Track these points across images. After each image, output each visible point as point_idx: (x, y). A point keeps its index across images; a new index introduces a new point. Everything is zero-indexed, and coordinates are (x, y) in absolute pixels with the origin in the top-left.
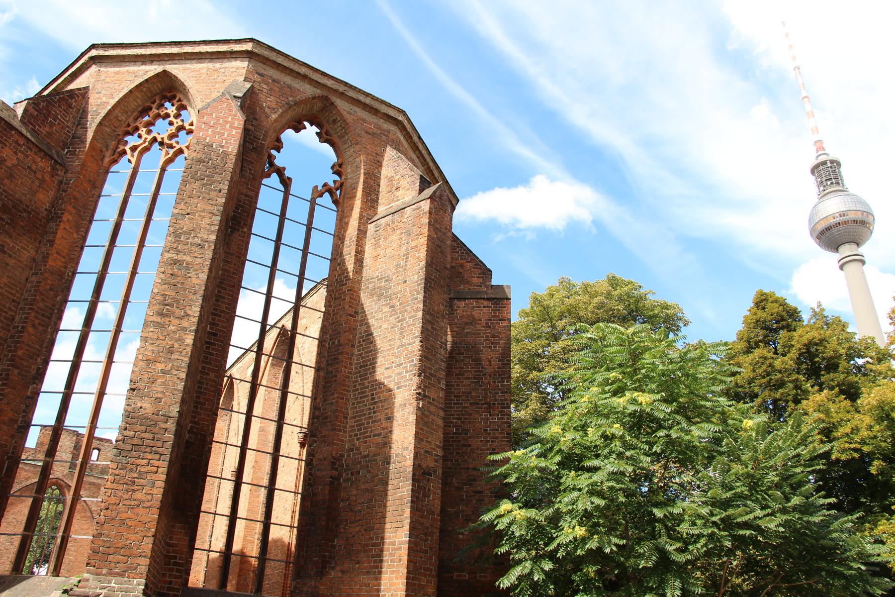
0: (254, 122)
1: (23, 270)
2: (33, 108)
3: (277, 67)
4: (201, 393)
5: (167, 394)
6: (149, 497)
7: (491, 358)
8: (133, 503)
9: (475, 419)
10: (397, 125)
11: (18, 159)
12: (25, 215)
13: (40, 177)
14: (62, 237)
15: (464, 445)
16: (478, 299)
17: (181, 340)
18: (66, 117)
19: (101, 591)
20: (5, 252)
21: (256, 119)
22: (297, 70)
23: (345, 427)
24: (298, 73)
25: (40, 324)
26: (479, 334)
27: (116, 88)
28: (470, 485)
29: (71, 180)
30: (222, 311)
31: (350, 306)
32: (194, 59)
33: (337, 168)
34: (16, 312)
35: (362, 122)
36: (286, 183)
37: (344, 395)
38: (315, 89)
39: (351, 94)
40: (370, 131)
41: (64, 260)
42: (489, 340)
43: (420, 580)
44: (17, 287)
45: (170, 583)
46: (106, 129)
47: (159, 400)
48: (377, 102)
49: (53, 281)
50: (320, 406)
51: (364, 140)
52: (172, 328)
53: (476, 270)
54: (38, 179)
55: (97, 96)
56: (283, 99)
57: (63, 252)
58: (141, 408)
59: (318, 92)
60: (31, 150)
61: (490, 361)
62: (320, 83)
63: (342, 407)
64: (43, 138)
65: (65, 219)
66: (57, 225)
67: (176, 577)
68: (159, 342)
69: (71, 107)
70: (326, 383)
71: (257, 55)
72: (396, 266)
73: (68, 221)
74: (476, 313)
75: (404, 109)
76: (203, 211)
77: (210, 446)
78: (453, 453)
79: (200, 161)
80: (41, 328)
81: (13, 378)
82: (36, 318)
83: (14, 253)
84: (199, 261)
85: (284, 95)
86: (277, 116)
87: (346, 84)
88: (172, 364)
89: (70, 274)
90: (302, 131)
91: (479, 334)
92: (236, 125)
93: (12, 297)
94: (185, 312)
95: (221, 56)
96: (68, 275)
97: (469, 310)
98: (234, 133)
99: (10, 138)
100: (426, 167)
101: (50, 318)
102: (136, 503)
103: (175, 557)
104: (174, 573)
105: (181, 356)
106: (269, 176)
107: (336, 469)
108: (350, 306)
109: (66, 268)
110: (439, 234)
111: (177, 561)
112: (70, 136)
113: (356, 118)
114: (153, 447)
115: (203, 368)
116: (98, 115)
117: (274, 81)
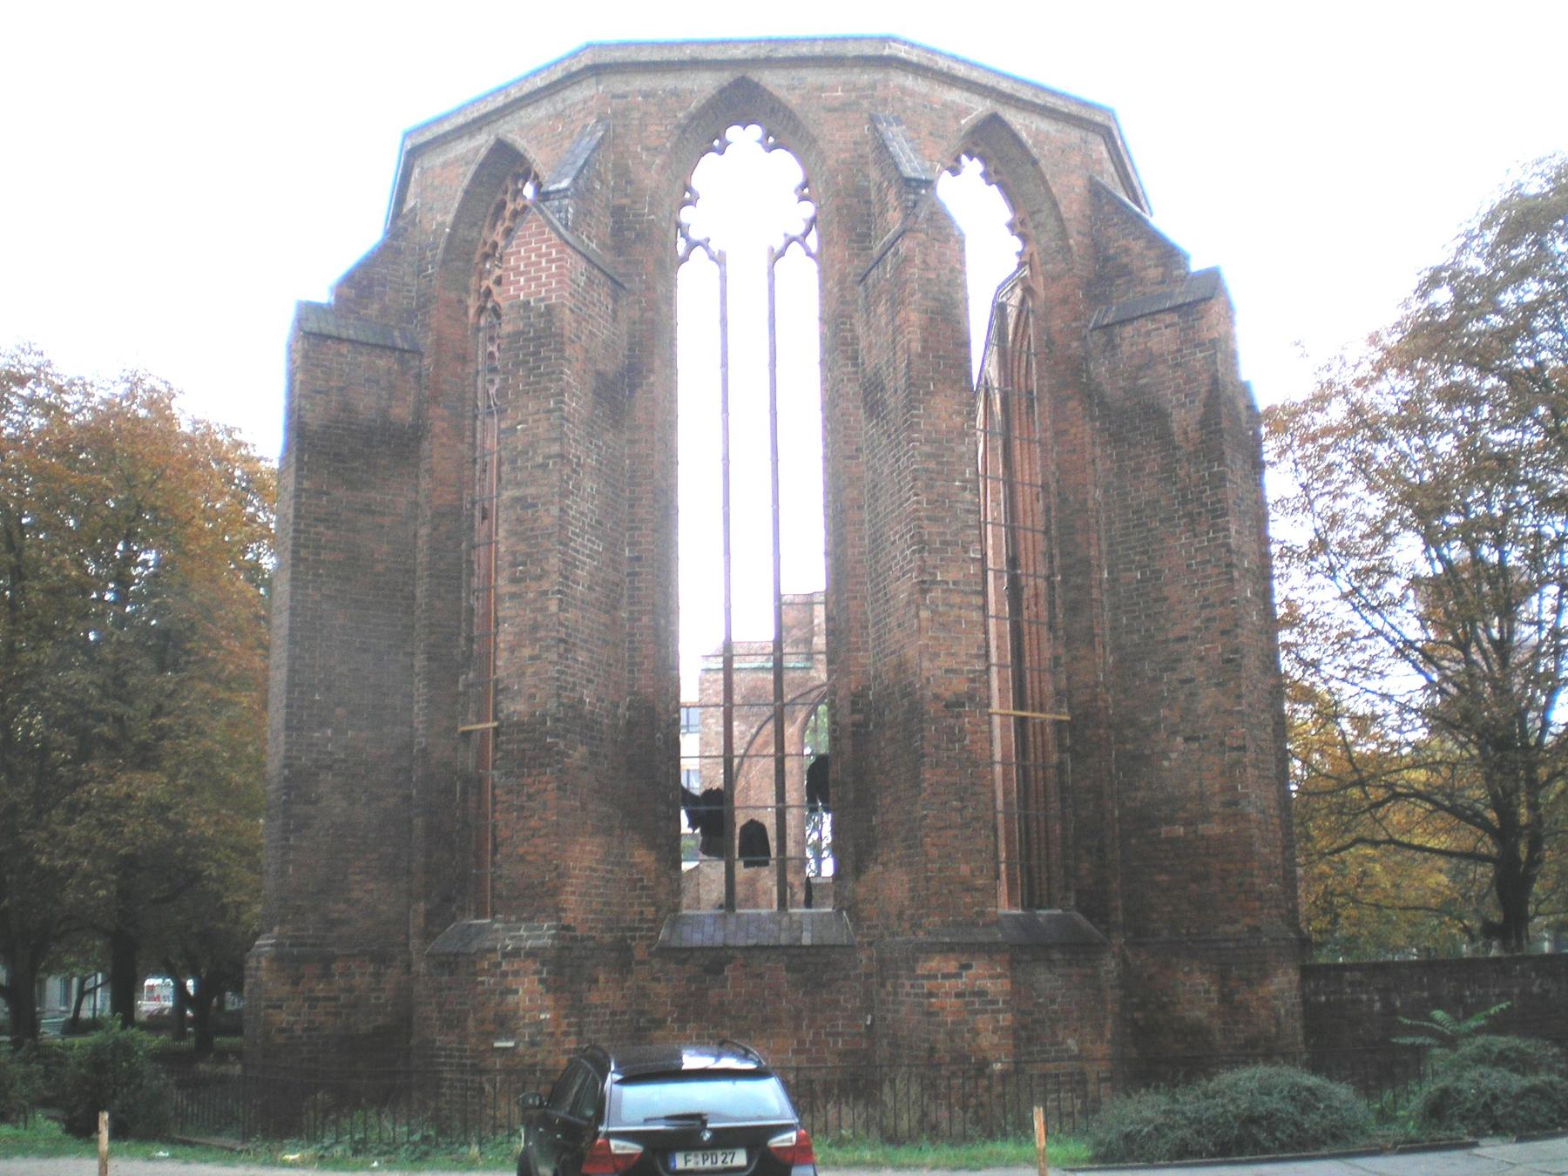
0: (629, 190)
4: (634, 649)
9: (1171, 548)
15: (1156, 601)
17: (544, 609)
21: (629, 182)
23: (867, 642)
26: (1164, 383)
28: (1173, 669)
30: (642, 521)
36: (719, 259)
38: (719, 74)
40: (837, 104)
42: (1181, 392)
47: (533, 696)
52: (531, 595)
53: (1151, 254)
55: (429, 216)
59: (726, 77)
65: (437, 430)
74: (1154, 344)
76: (537, 412)
78: (1139, 617)
84: (546, 489)
88: (541, 647)
91: (1164, 383)
94: (543, 570)
101: (459, 578)
103: (641, 880)
106: (685, 259)
107: (861, 711)
109: (461, 499)
115: (631, 613)
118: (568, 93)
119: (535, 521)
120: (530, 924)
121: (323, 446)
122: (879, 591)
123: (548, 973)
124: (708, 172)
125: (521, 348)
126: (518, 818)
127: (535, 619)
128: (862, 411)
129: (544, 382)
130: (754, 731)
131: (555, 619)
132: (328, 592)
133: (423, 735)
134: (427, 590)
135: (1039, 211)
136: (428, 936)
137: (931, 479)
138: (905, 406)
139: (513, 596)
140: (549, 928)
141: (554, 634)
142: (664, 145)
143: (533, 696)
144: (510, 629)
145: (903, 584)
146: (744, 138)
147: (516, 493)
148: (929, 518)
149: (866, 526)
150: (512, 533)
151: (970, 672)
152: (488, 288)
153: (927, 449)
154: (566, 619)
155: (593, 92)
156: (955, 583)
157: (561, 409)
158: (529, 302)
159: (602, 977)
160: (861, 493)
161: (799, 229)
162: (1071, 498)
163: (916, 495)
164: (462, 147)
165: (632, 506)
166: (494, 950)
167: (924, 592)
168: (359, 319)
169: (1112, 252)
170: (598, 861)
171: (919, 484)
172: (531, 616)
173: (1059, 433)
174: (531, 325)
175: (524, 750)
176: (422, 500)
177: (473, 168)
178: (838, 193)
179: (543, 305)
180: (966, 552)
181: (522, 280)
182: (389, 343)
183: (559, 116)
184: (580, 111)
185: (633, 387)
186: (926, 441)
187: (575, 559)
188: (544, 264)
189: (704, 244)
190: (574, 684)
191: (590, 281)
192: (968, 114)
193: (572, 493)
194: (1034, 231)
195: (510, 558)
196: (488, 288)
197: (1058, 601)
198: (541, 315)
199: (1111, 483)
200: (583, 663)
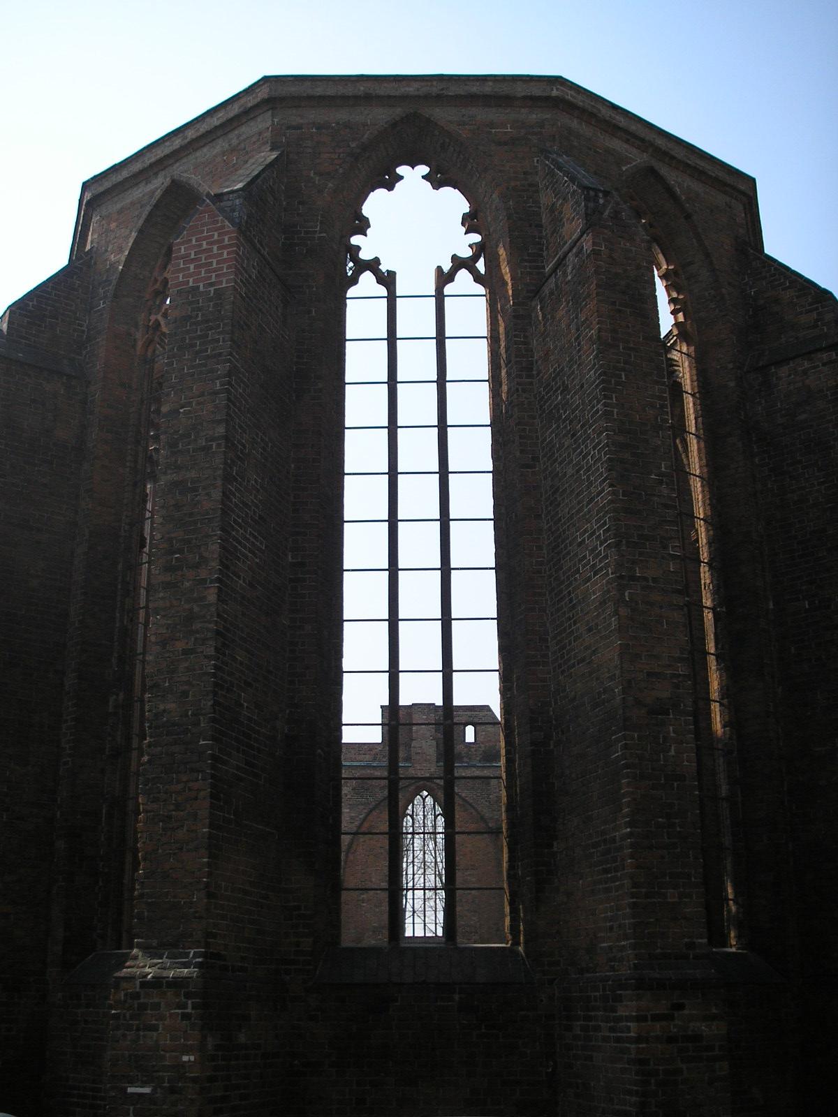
16: (810, 353)
22: (350, 94)
24: (356, 97)
29: (96, 394)
31: (522, 452)
32: (204, 146)
35: (488, 129)
36: (387, 280)
47: (185, 694)
56: (341, 150)
59: (398, 111)
62: (395, 97)
71: (282, 99)
75: (259, 77)
76: (202, 395)
77: (339, 733)
88: (196, 639)
92: (226, 242)
94: (201, 557)
96: (125, 531)
98: (225, 256)
100: (650, 150)
105: (206, 622)
106: (354, 281)
112: (83, 331)
118: (243, 129)
124: (376, 204)
140: (195, 956)
141: (212, 626)
143: (185, 694)
145: (596, 583)
158: (198, 287)
161: (467, 253)
164: (137, 193)
166: (131, 978)
169: (762, 302)
177: (148, 208)
179: (212, 289)
180: (665, 547)
181: (192, 266)
183: (233, 150)
189: (373, 265)
192: (630, 163)
198: (210, 300)
200: (241, 663)
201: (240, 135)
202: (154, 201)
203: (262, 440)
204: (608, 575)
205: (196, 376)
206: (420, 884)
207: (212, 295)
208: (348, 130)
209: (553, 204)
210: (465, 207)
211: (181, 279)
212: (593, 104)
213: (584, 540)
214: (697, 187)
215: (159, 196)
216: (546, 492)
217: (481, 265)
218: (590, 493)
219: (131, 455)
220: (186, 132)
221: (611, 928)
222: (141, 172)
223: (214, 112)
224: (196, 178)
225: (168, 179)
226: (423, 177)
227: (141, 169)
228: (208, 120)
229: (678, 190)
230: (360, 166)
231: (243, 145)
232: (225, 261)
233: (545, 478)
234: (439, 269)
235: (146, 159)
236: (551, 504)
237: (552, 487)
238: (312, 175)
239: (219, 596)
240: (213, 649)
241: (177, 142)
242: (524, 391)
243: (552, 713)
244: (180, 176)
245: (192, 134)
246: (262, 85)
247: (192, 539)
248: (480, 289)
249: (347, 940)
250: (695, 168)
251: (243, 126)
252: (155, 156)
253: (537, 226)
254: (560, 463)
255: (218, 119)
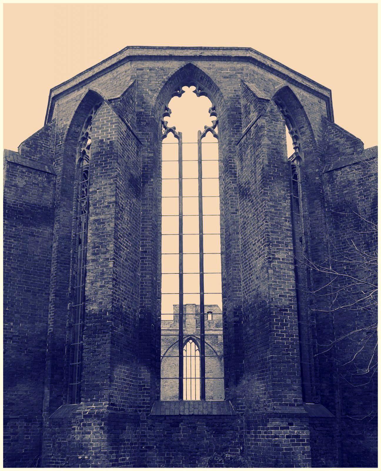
1: (48, 242)
2: (27, 146)
3: (150, 58)
4: (143, 289)
5: (105, 298)
6: (104, 357)
7: (365, 208)
8: (97, 362)
10: (248, 61)
11: (25, 181)
12: (39, 211)
13: (42, 186)
14: (64, 216)
18: (48, 143)
19: (87, 410)
20: (34, 236)
21: (144, 103)
22: (163, 55)
23: (240, 288)
25: (64, 269)
27: (69, 113)
30: (147, 237)
31: (232, 207)
33: (212, 111)
34: (50, 266)
35: (220, 71)
36: (178, 136)
37: (237, 267)
38: (181, 62)
39: (206, 53)
40: (227, 75)
41: (68, 229)
43: (285, 381)
44: (47, 252)
45: (144, 400)
46: (72, 141)
47: (101, 303)
48: (228, 51)
49: (65, 243)
50: (226, 277)
51: (223, 84)
52: (101, 260)
53: (348, 143)
54: (41, 187)
55: (61, 122)
57: (66, 224)
58: (93, 309)
59: (183, 63)
60: (31, 173)
61: (365, 211)
62: (182, 56)
63: (236, 275)
64: (37, 162)
66: (59, 210)
67: (146, 396)
68: (95, 271)
69: (49, 136)
70: (227, 261)
72: (251, 171)
73: (64, 205)
79: (98, 153)
80: (65, 271)
81: (57, 302)
82: (61, 266)
83: (39, 234)
84: (109, 216)
85: (159, 77)
86: (158, 94)
87: (201, 48)
88: (105, 281)
89: (74, 236)
90: (182, 95)
91: (355, 192)
92: (114, 121)
93: (46, 259)
94: (107, 249)
95: (115, 67)
97: (345, 176)
98: (114, 127)
99: (17, 171)
101: (69, 264)
102: (98, 361)
103: (144, 386)
104: (145, 394)
105: (108, 275)
106: (165, 136)
107: (238, 316)
108: (232, 207)
110: (274, 140)
111: (146, 387)
112: (53, 154)
113: (215, 70)
114: (102, 330)
115: (142, 274)
116: (64, 134)
117: (150, 70)
118: (119, 69)
119: (104, 229)
120: (97, 403)
121: (14, 207)
122: (247, 266)
123: (104, 425)
125: (99, 159)
126: (93, 356)
127: (103, 270)
128: (238, 195)
129: (109, 172)
130: (165, 351)
131: (111, 270)
132: (14, 266)
133: (52, 327)
134: (56, 268)
135: (303, 127)
136: (51, 411)
137: (273, 216)
138: (261, 187)
139: (93, 261)
141: (111, 276)
142: (158, 89)
144: (92, 275)
146: (189, 91)
147: (96, 218)
148: (272, 232)
149: (240, 240)
150: (93, 234)
151: (289, 296)
152: (84, 151)
153: (271, 203)
154: (116, 271)
155: (129, 67)
156: (283, 259)
157: (116, 183)
158: (103, 140)
159: (127, 427)
160: (238, 227)
161: (211, 125)
162: (316, 238)
163: (266, 222)
165: (143, 231)
166: (80, 414)
167: (270, 262)
168: (31, 160)
169: (331, 144)
170: (127, 377)
171: (268, 217)
172: (101, 269)
173: (311, 213)
174: (104, 149)
175: (96, 326)
176: (54, 232)
177: (79, 102)
178: (228, 110)
179: (109, 141)
181: (100, 131)
182: (43, 170)
183: (115, 78)
184: (123, 76)
185: (144, 183)
186: (270, 200)
187: (120, 247)
188: (109, 125)
189: (172, 130)
190: (119, 299)
191: (128, 136)
193: (120, 219)
194: (300, 135)
195: (92, 245)
196: (84, 151)
197: (311, 279)
198: (108, 145)
199: (332, 232)
200: (122, 291)
201: (117, 72)
202: (81, 99)
203: (129, 202)
204: (265, 257)
205: (103, 177)
206: (193, 358)
207: (109, 143)
208: (162, 71)
209: (246, 105)
210: (210, 105)
211: (96, 137)
212: (264, 59)
213: (255, 243)
214: (306, 94)
215: (83, 97)
216: (241, 224)
217: (216, 130)
218: (258, 224)
219: (75, 206)
220: (94, 69)
221: (265, 393)
222: (76, 86)
223: (106, 61)
224: (99, 90)
225: (87, 89)
226: (193, 92)
227: (75, 84)
228: (103, 64)
229: (298, 96)
230: (167, 87)
231: (118, 77)
232: (113, 129)
233: (241, 218)
234: (200, 132)
235: (77, 80)
236: (243, 229)
237: (243, 221)
238: (148, 90)
239: (114, 265)
240: (112, 285)
241: (91, 73)
242: (233, 183)
243: (242, 310)
244: (92, 88)
245: (97, 70)
246: (126, 50)
247: (103, 242)
248: (216, 140)
249: (162, 399)
250: (306, 86)
251: (119, 68)
252: (81, 79)
253: (239, 113)
254: (247, 212)
255: (108, 64)
